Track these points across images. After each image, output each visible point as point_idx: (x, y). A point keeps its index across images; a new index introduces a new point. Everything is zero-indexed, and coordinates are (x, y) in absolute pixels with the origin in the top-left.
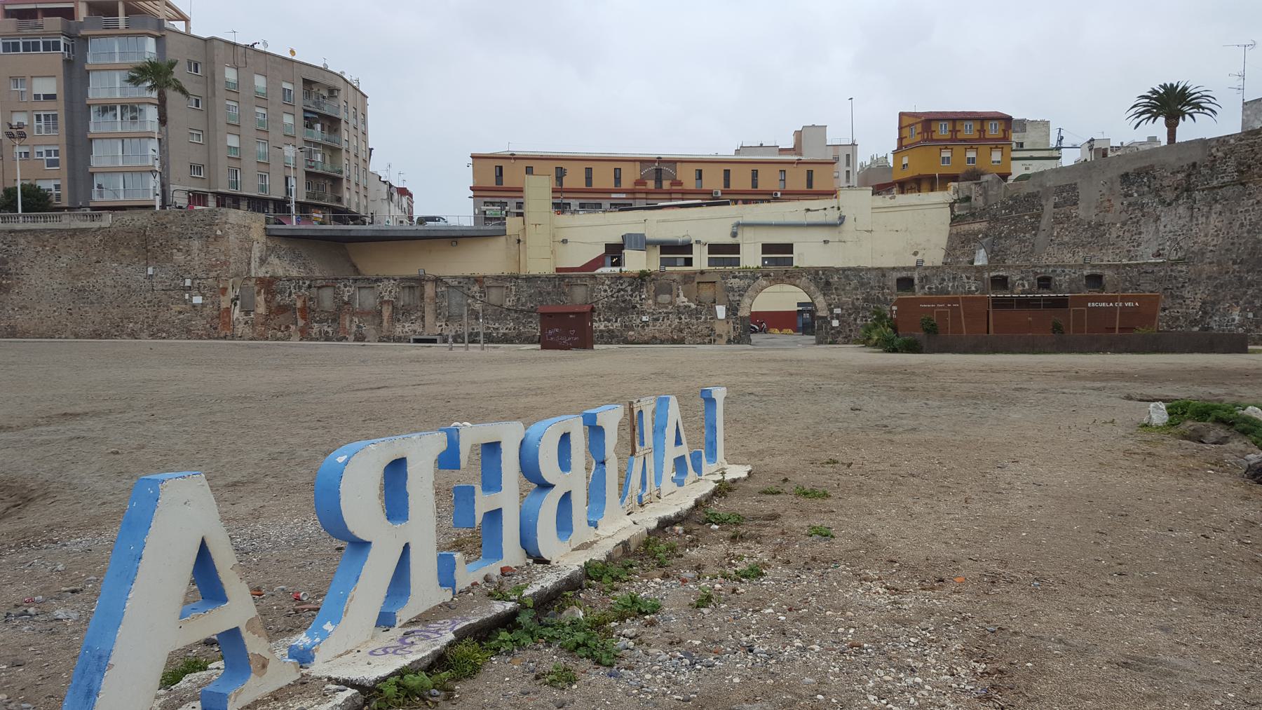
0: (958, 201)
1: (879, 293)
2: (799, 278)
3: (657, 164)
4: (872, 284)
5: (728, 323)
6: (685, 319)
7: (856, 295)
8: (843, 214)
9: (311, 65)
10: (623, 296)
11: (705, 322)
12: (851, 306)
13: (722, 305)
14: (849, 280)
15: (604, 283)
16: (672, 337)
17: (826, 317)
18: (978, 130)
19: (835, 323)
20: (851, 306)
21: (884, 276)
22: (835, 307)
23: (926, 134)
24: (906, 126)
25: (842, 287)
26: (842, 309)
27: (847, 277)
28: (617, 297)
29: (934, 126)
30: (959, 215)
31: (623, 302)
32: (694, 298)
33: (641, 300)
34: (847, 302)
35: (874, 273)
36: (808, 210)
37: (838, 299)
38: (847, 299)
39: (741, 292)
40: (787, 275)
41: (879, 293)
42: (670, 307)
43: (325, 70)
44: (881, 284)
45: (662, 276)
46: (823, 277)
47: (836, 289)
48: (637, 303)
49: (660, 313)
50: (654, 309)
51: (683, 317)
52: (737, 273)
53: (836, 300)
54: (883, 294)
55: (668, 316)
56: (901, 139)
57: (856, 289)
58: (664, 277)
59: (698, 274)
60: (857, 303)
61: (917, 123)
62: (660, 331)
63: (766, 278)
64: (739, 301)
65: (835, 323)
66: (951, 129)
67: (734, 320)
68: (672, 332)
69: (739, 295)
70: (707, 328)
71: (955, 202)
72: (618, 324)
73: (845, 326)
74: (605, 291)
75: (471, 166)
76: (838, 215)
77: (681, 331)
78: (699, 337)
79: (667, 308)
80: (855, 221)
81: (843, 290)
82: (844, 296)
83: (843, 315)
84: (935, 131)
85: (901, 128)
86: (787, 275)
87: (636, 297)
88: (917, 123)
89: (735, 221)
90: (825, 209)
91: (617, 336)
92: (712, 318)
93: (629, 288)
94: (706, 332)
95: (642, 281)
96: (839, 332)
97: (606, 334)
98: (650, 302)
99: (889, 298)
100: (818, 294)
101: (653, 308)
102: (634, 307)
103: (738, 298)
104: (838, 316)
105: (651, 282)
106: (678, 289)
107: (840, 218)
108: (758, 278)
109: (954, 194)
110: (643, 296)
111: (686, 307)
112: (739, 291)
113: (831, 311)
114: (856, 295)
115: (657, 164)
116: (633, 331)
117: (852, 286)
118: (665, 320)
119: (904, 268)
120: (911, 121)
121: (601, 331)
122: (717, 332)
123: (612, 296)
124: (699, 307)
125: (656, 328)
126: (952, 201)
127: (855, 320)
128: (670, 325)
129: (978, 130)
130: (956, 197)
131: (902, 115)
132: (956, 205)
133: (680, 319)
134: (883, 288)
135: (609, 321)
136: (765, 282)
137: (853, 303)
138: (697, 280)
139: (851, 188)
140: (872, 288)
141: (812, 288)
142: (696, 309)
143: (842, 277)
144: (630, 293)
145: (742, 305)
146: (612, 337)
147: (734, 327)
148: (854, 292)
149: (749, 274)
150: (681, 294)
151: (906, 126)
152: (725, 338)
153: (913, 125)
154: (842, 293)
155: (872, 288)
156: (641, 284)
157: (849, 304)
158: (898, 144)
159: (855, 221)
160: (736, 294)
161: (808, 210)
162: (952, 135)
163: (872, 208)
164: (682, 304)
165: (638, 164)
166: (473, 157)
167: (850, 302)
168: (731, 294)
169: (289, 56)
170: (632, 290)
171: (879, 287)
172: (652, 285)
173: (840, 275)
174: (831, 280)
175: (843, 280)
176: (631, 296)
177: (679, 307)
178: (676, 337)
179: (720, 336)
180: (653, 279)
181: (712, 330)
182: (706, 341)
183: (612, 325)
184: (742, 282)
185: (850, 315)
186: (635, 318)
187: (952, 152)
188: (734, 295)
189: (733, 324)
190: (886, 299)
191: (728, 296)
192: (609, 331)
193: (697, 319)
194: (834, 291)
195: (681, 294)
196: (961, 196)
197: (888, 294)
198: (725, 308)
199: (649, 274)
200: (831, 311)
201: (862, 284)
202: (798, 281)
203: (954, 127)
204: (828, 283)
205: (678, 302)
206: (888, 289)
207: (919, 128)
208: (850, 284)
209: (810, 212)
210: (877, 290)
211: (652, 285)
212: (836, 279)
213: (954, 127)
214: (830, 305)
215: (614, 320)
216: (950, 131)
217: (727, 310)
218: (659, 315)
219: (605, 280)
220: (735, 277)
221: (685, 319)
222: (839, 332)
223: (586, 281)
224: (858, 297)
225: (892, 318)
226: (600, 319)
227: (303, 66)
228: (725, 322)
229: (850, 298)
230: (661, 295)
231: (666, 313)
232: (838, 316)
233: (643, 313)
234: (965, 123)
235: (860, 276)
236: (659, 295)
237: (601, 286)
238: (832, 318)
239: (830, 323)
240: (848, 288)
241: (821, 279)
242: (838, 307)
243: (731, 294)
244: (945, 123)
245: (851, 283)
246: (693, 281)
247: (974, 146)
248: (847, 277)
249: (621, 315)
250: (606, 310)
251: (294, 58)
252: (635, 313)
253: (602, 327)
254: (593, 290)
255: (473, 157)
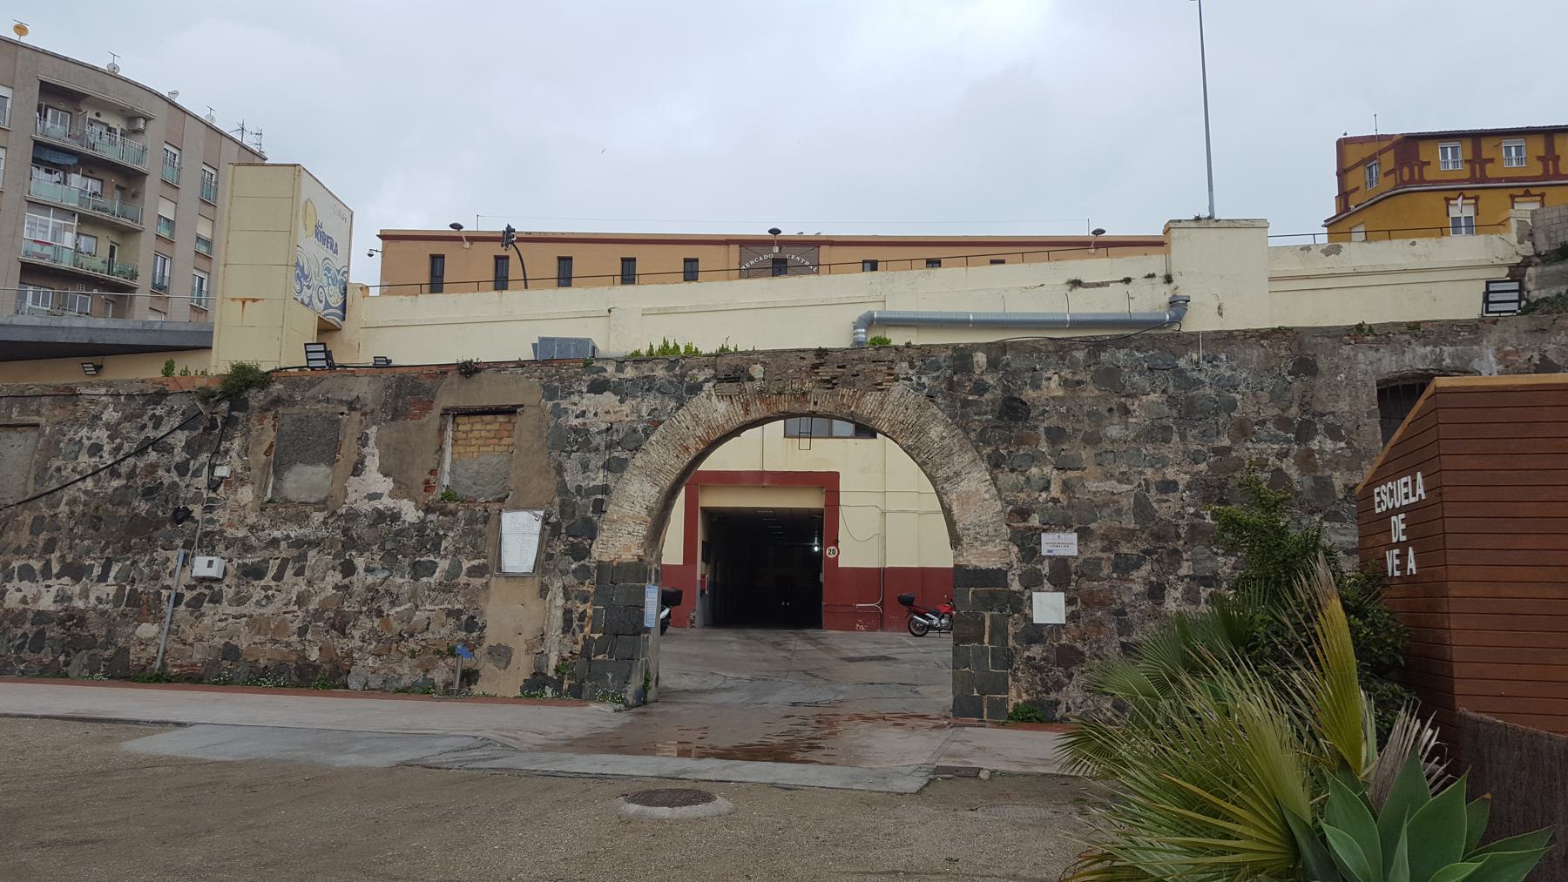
0: (1537, 260)
1: (1281, 456)
2: (877, 386)
3: (776, 249)
4: (1245, 407)
5: (544, 591)
6: (369, 570)
7: (1161, 462)
8: (1182, 293)
9: (66, 59)
10: (152, 469)
11: (447, 587)
12: (1130, 523)
13: (529, 508)
14: (1119, 390)
15: (97, 417)
16: (302, 656)
17: (995, 577)
18: (1539, 158)
19: (1048, 607)
20: (1130, 523)
21: (1305, 367)
22: (1048, 526)
23: (1406, 170)
24: (1357, 165)
25: (1087, 426)
26: (1084, 535)
27: (1110, 378)
28: (131, 475)
29: (1425, 152)
30: (1538, 302)
31: (148, 493)
32: (419, 476)
33: (214, 485)
34: (1111, 499)
35: (1255, 354)
36: (1076, 283)
37: (1066, 486)
38: (1111, 485)
39: (618, 453)
40: (825, 373)
41: (1281, 456)
42: (318, 517)
43: (112, 74)
44: (1294, 411)
45: (312, 384)
46: (990, 379)
47: (1055, 435)
48: (197, 499)
49: (274, 543)
50: (252, 528)
51: (360, 563)
52: (610, 369)
53: (1055, 491)
54: (1306, 461)
55: (303, 557)
56: (1344, 196)
57: (1157, 433)
58: (313, 391)
59: (453, 377)
60: (1165, 508)
61: (1380, 153)
62: (255, 624)
63: (734, 388)
64: (605, 490)
65: (1048, 607)
66: (1470, 157)
67: (570, 580)
68: (302, 632)
69: (607, 466)
70: (450, 613)
71: (1527, 262)
72: (108, 590)
73: (1099, 624)
74: (96, 449)
75: (378, 257)
76: (1169, 295)
77: (340, 626)
78: (413, 654)
79: (301, 519)
80: (1221, 314)
81: (1092, 440)
82: (1091, 468)
83: (1090, 568)
84: (1428, 163)
85: (1342, 173)
86: (825, 373)
87: (197, 473)
88: (1380, 153)
89: (861, 311)
90: (1127, 280)
91: (91, 643)
92: (475, 572)
93: (181, 438)
94: (443, 631)
95: (232, 408)
96: (1068, 658)
97: (54, 632)
98: (246, 494)
99: (1339, 480)
100: (962, 460)
101: (252, 519)
102: (183, 515)
103: (599, 478)
104: (1062, 575)
105: (264, 409)
106: (363, 440)
107: (1173, 303)
108: (695, 389)
109: (1520, 242)
110: (221, 472)
111: (380, 516)
112: (609, 447)
113: (1027, 544)
114: (1161, 462)
115: (776, 249)
116: (158, 619)
117: (1139, 418)
118: (289, 572)
119: (1414, 327)
120: (1366, 151)
121: (41, 617)
122: (492, 637)
123: (113, 472)
124: (432, 517)
125: (249, 608)
126: (1518, 260)
127: (1156, 592)
128: (301, 600)
129: (1539, 158)
130: (1527, 249)
131: (1343, 145)
132: (1531, 271)
133: (348, 569)
134: (1304, 432)
135: (75, 571)
136: (722, 407)
137: (1142, 508)
138: (445, 400)
139: (1202, 223)
140: (1243, 430)
141: (936, 432)
142: (421, 527)
143: (1084, 376)
144: (179, 456)
145: (612, 511)
146: (73, 645)
147: (567, 613)
148: (1148, 449)
149: (660, 372)
150: (373, 463)
151: (1357, 165)
152: (522, 667)
153: (1372, 158)
154: (1086, 454)
155: (1243, 430)
156: (229, 422)
157: (1119, 512)
158: (1338, 205)
159: (1221, 314)
160: (596, 461)
161: (1076, 283)
162: (1473, 171)
163: (1271, 279)
164: (366, 506)
165: (735, 249)
166: (385, 237)
167: (1127, 503)
168: (572, 463)
169: (15, 37)
170: (188, 446)
171: (1283, 423)
172: (268, 422)
173: (1074, 365)
174: (1029, 394)
175: (1091, 391)
176: (182, 469)
177: (353, 516)
178: (314, 655)
179: (501, 655)
180: (277, 401)
181: (471, 625)
182: (439, 676)
183: (85, 594)
184: (626, 408)
185: (1124, 566)
186: (171, 566)
187: (1476, 205)
188: (585, 467)
189: (567, 597)
190: (1323, 486)
191: (560, 470)
192: (74, 619)
193: (419, 570)
194: (1044, 447)
195: (373, 463)
196: (1543, 247)
197: (1335, 462)
198: (537, 526)
199: (263, 380)
200: (1027, 544)
201: (1189, 412)
202: (870, 402)
203: (1477, 151)
204: (1014, 410)
205: (352, 496)
206: (1334, 433)
207: (1388, 160)
208: (1126, 411)
209: (1080, 290)
210: (1273, 439)
211: (268, 422)
212: (1054, 387)
213: (1477, 151)
214: (1023, 513)
215: (97, 571)
216: (1466, 161)
217: (550, 531)
218: (266, 554)
219: (105, 407)
220: (598, 387)
221: (369, 570)
222: (1068, 658)
223: (38, 413)
224: (1170, 473)
225: (1375, 577)
226: (48, 565)
227: (45, 57)
228: (531, 588)
229: (1124, 478)
230: (299, 468)
231: (298, 543)
232: (1062, 575)
233: (208, 542)
234: (1505, 143)
235: (1180, 373)
236: (292, 463)
237: (84, 432)
238: (1033, 581)
239: (1019, 604)
240: (1114, 431)
241: (980, 388)
242: (1066, 526)
243: (572, 463)
244: (1455, 144)
245: (1134, 405)
246: (427, 406)
247: (1533, 191)
248: (1110, 378)
249: (127, 549)
250: (78, 530)
251: (24, 40)
252: (179, 542)
253: (47, 603)
254: (52, 448)
255: (385, 237)
